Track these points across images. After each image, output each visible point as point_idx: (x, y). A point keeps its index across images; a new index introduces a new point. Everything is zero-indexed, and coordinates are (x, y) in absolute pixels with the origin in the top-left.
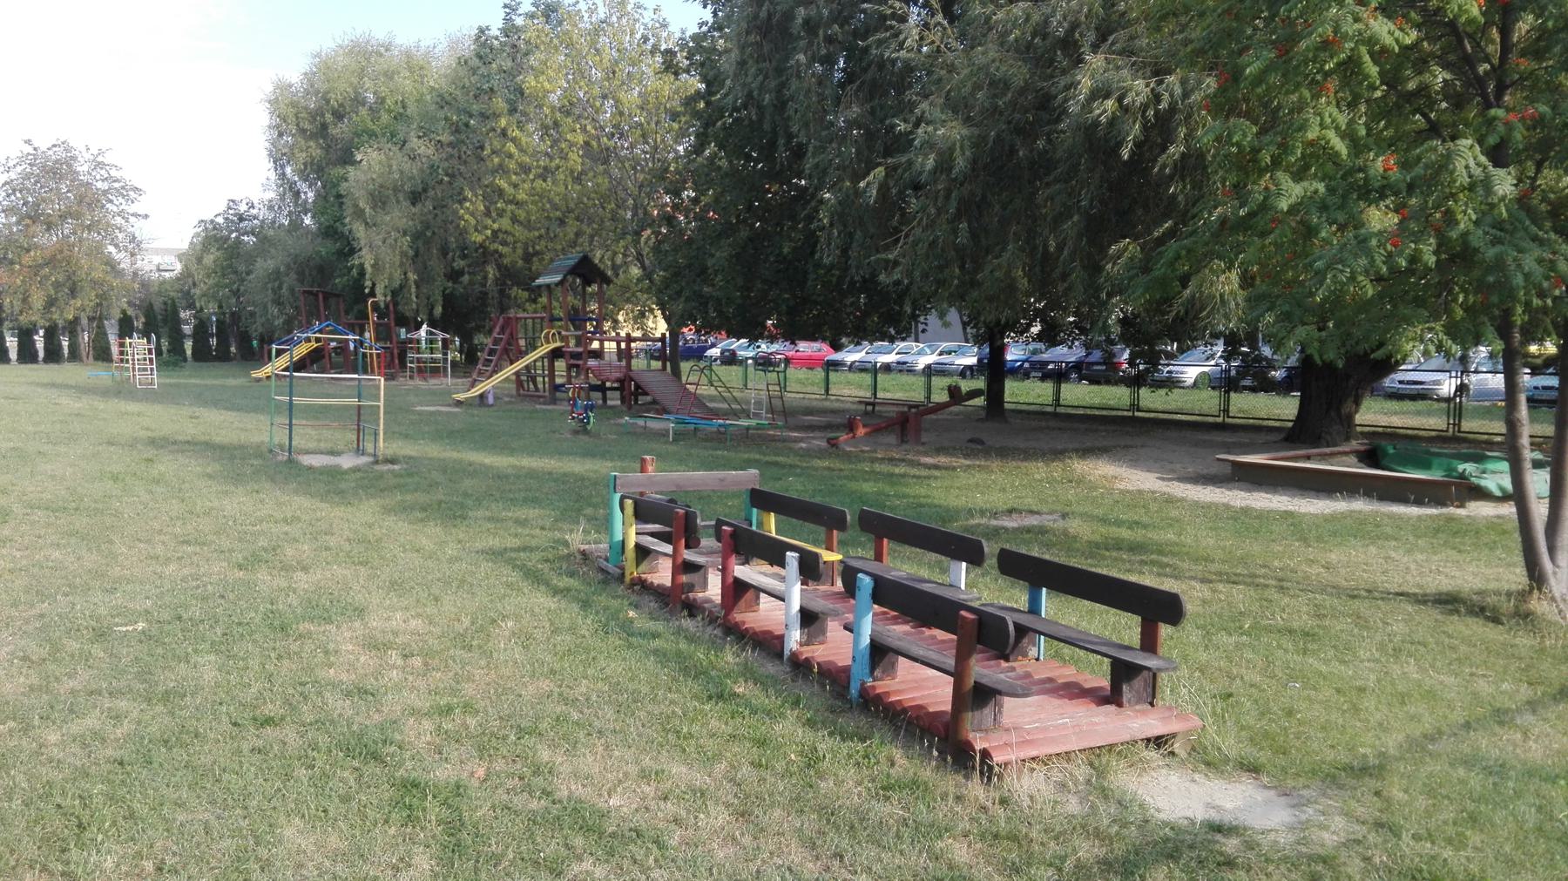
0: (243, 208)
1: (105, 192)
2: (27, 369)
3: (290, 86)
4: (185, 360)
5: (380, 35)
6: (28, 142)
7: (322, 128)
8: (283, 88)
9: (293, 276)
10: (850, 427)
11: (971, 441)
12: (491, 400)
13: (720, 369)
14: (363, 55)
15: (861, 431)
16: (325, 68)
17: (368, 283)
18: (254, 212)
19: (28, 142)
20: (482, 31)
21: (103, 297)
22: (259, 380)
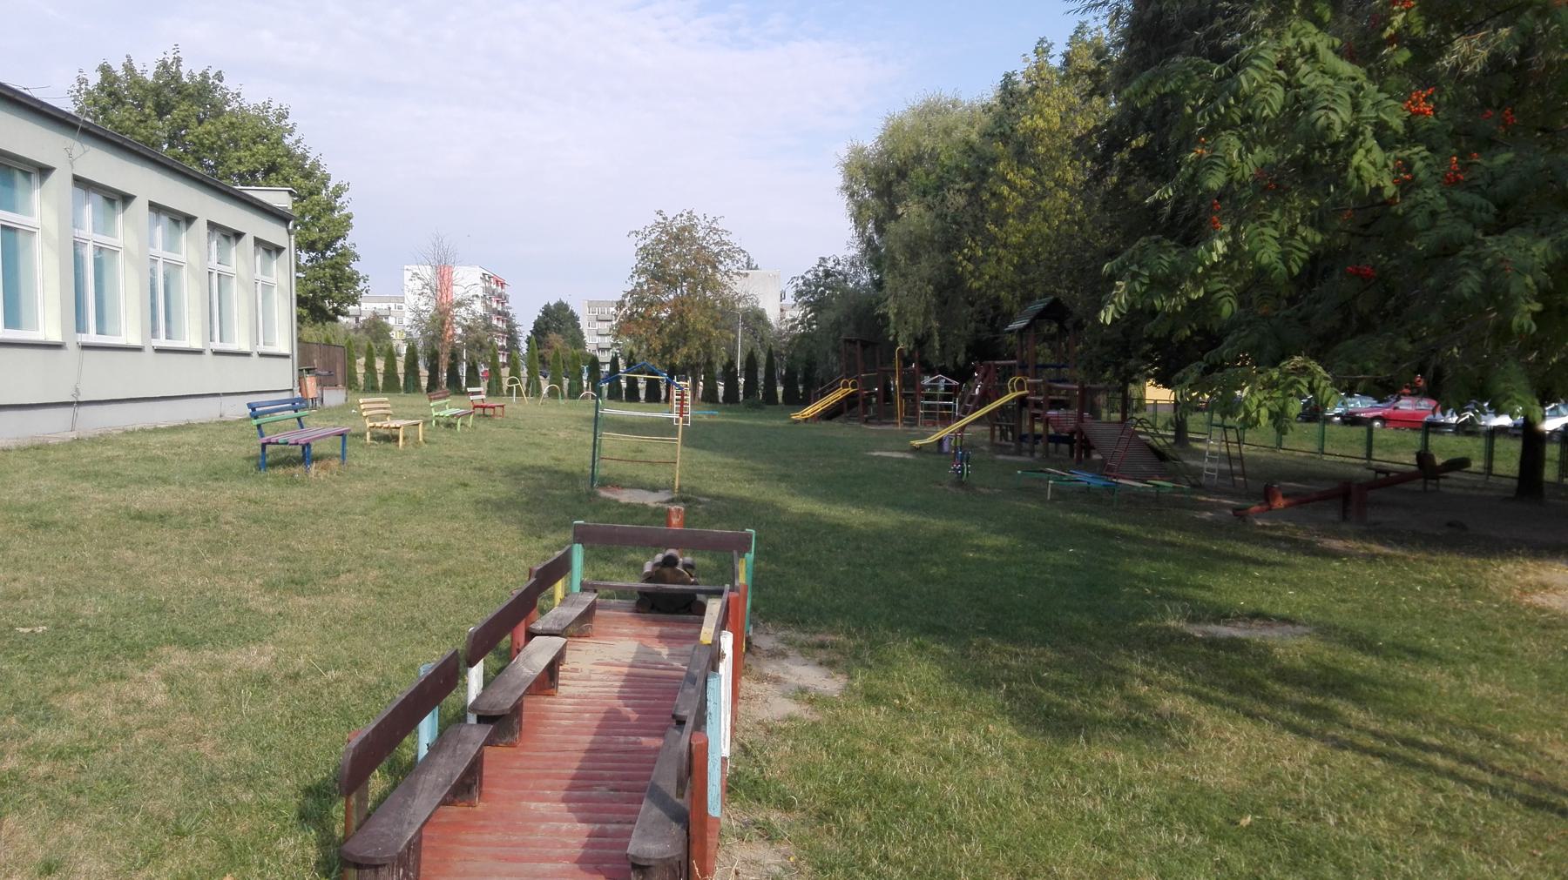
0: (830, 264)
1: (718, 254)
2: (552, 401)
3: (863, 149)
4: (776, 403)
5: (948, 94)
6: (660, 213)
7: (883, 183)
8: (858, 152)
9: (852, 326)
10: (1267, 495)
11: (1450, 525)
12: (946, 448)
13: (1336, 431)
14: (930, 111)
15: (1280, 503)
16: (894, 132)
17: (892, 331)
18: (839, 268)
19: (660, 213)
20: (1008, 76)
21: (706, 346)
22: (797, 422)
